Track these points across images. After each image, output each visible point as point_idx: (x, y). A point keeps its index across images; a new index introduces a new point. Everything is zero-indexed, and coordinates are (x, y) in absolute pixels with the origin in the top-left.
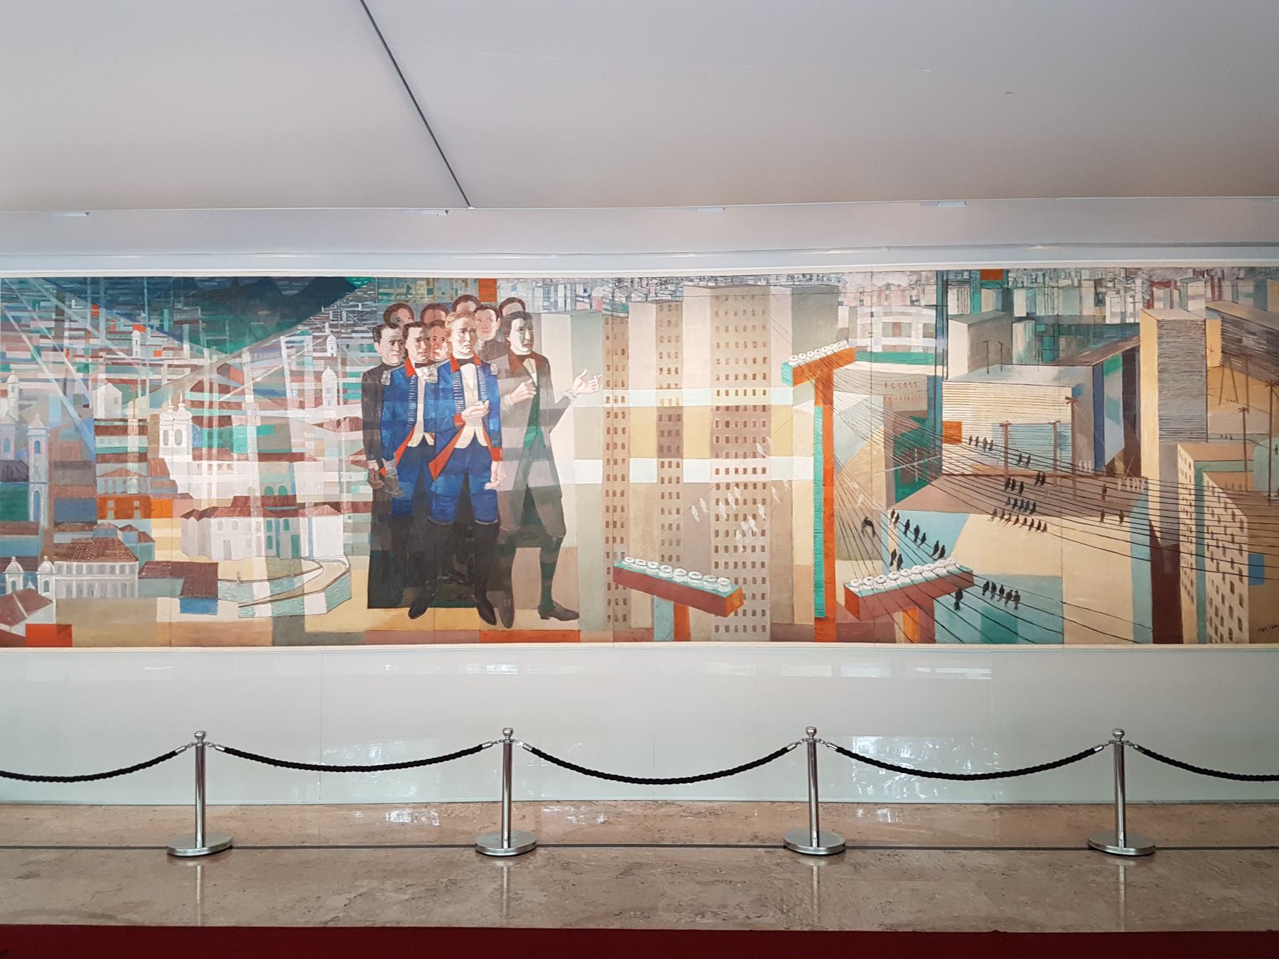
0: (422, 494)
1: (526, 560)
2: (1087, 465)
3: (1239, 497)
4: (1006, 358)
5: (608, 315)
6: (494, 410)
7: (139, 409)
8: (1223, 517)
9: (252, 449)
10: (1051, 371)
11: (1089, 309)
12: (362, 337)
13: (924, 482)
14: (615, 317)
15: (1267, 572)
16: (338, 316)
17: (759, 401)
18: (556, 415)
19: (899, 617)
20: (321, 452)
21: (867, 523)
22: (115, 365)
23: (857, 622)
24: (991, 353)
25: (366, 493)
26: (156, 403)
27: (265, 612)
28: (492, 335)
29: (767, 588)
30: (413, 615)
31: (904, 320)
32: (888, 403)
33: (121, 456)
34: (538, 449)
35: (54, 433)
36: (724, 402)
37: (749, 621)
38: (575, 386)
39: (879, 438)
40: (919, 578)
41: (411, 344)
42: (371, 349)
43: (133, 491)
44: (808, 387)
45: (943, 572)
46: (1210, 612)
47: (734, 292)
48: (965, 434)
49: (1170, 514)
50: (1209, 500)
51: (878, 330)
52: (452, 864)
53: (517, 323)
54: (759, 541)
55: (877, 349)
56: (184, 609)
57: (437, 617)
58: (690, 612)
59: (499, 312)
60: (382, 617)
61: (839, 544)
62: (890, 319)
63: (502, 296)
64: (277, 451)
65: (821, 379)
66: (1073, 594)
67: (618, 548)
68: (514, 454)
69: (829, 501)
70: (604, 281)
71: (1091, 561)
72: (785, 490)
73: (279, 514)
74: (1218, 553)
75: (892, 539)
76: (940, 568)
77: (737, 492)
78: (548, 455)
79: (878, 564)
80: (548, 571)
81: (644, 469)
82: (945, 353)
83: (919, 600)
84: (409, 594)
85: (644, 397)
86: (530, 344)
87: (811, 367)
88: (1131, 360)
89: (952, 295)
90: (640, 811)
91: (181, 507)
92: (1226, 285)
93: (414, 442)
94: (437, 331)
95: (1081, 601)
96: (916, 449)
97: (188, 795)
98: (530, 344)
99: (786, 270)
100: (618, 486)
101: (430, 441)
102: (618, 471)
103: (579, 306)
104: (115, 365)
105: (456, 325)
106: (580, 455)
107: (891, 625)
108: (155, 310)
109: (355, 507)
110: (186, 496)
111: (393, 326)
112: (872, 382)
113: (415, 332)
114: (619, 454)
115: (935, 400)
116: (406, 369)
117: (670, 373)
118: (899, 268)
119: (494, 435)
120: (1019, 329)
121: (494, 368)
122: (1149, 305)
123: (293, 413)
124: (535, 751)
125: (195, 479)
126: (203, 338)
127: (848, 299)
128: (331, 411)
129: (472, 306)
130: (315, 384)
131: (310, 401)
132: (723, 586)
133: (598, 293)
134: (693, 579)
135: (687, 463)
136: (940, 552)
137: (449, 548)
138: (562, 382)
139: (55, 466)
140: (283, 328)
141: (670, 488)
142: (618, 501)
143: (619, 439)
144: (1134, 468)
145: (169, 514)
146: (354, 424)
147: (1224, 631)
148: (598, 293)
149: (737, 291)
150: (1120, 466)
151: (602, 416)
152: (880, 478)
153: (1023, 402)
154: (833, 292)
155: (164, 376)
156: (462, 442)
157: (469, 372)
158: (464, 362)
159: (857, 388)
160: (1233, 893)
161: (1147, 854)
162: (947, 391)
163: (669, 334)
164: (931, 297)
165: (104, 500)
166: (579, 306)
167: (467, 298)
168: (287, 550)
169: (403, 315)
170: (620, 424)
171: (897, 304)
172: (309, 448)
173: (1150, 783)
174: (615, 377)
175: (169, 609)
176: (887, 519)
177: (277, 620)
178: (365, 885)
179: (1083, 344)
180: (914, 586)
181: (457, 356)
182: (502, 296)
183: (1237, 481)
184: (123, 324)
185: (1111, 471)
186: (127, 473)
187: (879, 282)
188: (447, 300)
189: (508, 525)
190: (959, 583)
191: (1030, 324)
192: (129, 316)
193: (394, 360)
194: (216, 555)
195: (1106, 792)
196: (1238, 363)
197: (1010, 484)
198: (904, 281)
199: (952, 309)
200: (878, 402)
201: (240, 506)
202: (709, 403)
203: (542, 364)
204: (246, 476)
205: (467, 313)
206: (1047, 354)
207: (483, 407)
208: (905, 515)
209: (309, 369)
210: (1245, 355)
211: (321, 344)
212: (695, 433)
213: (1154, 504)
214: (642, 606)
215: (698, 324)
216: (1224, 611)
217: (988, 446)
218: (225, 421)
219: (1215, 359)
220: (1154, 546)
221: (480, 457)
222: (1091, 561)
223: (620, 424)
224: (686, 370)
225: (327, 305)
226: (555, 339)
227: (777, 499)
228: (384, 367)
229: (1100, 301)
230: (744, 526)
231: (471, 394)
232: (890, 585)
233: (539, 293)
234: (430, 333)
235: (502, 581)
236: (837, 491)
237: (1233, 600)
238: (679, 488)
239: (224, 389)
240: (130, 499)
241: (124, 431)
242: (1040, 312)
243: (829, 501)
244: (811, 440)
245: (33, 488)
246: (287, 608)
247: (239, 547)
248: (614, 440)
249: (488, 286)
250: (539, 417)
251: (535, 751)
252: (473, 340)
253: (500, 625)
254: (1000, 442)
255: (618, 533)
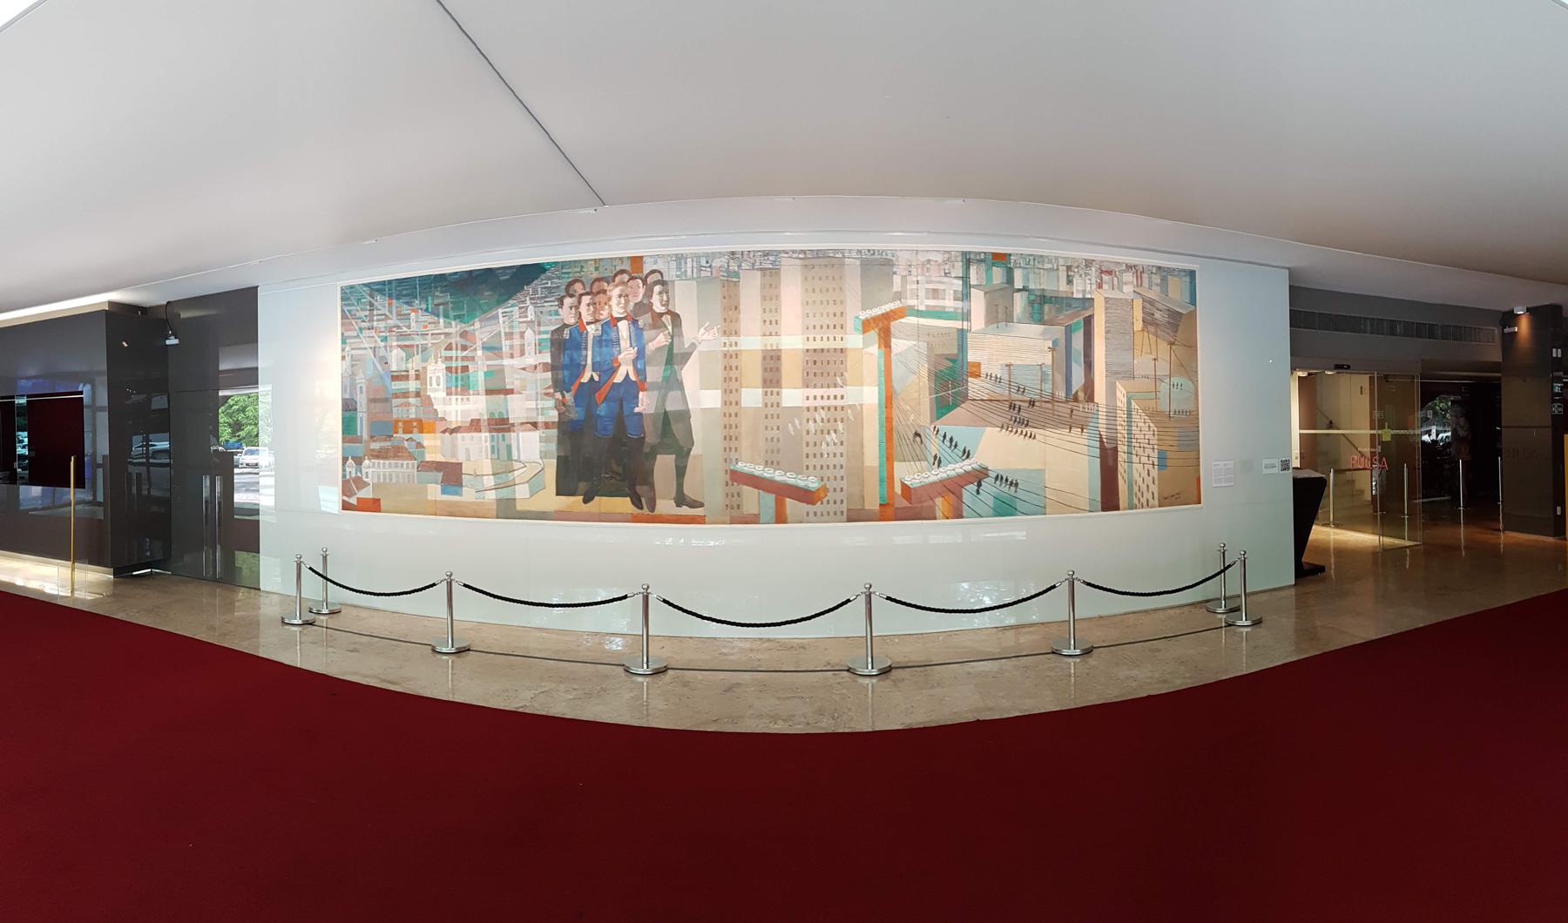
0: (590, 416)
1: (664, 464)
2: (1061, 394)
3: (1154, 415)
4: (1009, 318)
5: (724, 281)
6: (641, 354)
7: (414, 364)
8: (1144, 429)
9: (481, 388)
10: (1039, 328)
11: (1063, 287)
12: (551, 305)
13: (956, 405)
14: (730, 282)
15: (1169, 462)
16: (535, 292)
17: (838, 345)
18: (686, 356)
19: (939, 501)
20: (524, 388)
21: (917, 434)
22: (402, 336)
23: (908, 506)
24: (999, 315)
25: (554, 416)
26: (425, 360)
27: (492, 495)
28: (639, 299)
29: (844, 484)
30: (586, 501)
31: (940, 287)
32: (930, 348)
33: (405, 394)
34: (673, 383)
35: (369, 381)
36: (812, 345)
37: (831, 508)
38: (700, 335)
39: (924, 373)
40: (952, 473)
41: (583, 309)
42: (557, 313)
43: (413, 416)
44: (873, 334)
45: (969, 468)
46: (1136, 489)
47: (819, 263)
48: (984, 370)
49: (1112, 427)
50: (1135, 417)
51: (922, 294)
52: (606, 677)
53: (657, 288)
54: (840, 449)
55: (922, 308)
56: (443, 492)
57: (602, 503)
58: (788, 500)
59: (644, 281)
60: (565, 502)
61: (897, 450)
62: (931, 286)
63: (647, 269)
64: (497, 390)
65: (882, 328)
66: (1052, 481)
67: (733, 455)
68: (655, 386)
69: (889, 419)
70: (721, 254)
71: (1063, 458)
72: (858, 410)
73: (498, 431)
74: (1140, 451)
75: (934, 446)
76: (967, 466)
77: (823, 413)
78: (680, 386)
79: (925, 464)
80: (681, 472)
81: (752, 397)
82: (969, 312)
83: (952, 488)
84: (582, 486)
85: (752, 342)
86: (667, 304)
87: (875, 319)
88: (1088, 322)
89: (973, 270)
90: (748, 645)
91: (441, 426)
92: (1145, 276)
93: (585, 379)
94: (601, 297)
95: (1056, 486)
96: (951, 382)
97: (443, 612)
98: (667, 304)
99: (860, 246)
100: (733, 409)
101: (596, 378)
102: (733, 398)
103: (703, 274)
104: (402, 336)
105: (615, 292)
106: (706, 385)
107: (932, 508)
108: (424, 298)
109: (547, 425)
110: (443, 419)
111: (572, 296)
112: (919, 332)
113: (586, 299)
114: (733, 385)
115: (962, 347)
116: (580, 327)
117: (771, 325)
118: (936, 248)
119: (641, 372)
120: (1017, 296)
121: (641, 323)
122: (1100, 286)
123: (506, 362)
124: (665, 601)
125: (448, 408)
126: (452, 314)
127: (900, 269)
128: (530, 360)
129: (626, 277)
130: (519, 337)
131: (517, 351)
132: (812, 483)
133: (716, 263)
134: (789, 478)
135: (785, 392)
136: (966, 454)
137: (611, 455)
138: (691, 331)
139: (372, 401)
140: (501, 302)
141: (772, 410)
142: (733, 420)
143: (733, 374)
144: (1090, 397)
145: (434, 431)
146: (546, 367)
147: (1144, 500)
148: (716, 263)
149: (825, 261)
150: (1081, 395)
151: (720, 356)
152: (926, 402)
153: (1014, 351)
154: (888, 263)
155: (429, 341)
156: (619, 378)
157: (623, 326)
158: (620, 319)
159: (907, 337)
160: (1134, 672)
161: (1087, 652)
162: (971, 340)
163: (770, 295)
164: (958, 270)
165: (397, 421)
166: (703, 274)
167: (622, 272)
168: (504, 455)
169: (578, 288)
170: (734, 362)
171: (935, 275)
172: (516, 385)
173: (1092, 605)
174: (730, 328)
175: (434, 492)
176: (930, 432)
177: (499, 501)
178: (547, 685)
179: (1059, 311)
180: (950, 479)
181: (616, 315)
182: (647, 269)
183: (1152, 404)
184: (405, 309)
185: (1076, 399)
186: (409, 404)
187: (922, 258)
188: (608, 274)
189: (651, 439)
190: (979, 476)
191: (1025, 294)
192: (408, 303)
193: (572, 321)
194: (461, 458)
195: (1063, 614)
196: (1152, 329)
197: (1012, 407)
198: (939, 258)
199: (973, 281)
200: (923, 345)
201: (475, 426)
202: (800, 346)
203: (676, 318)
204: (477, 405)
205: (623, 283)
206: (1036, 316)
207: (633, 352)
208: (943, 429)
209: (517, 330)
210: (1154, 323)
211: (524, 313)
212: (791, 369)
213: (1102, 421)
214: (750, 496)
215: (792, 291)
216: (1144, 488)
217: (998, 380)
218: (465, 369)
219: (1138, 325)
220: (1102, 448)
221: (632, 388)
222: (1063, 458)
223: (734, 362)
224: (784, 321)
225: (528, 283)
226: (685, 300)
227: (848, 417)
228: (566, 326)
229: (1070, 282)
230: (828, 438)
231: (624, 343)
232: (933, 479)
233: (673, 265)
234: (597, 299)
235: (647, 478)
236: (895, 412)
237: (1149, 480)
238: (778, 411)
239: (464, 348)
240: (411, 421)
241: (406, 378)
242: (1032, 287)
243: (889, 419)
244: (876, 373)
245: (359, 415)
246: (505, 493)
247: (474, 451)
248: (730, 374)
249: (637, 261)
250: (674, 358)
251: (665, 601)
252: (627, 302)
253: (646, 511)
254: (1006, 377)
255: (733, 444)
